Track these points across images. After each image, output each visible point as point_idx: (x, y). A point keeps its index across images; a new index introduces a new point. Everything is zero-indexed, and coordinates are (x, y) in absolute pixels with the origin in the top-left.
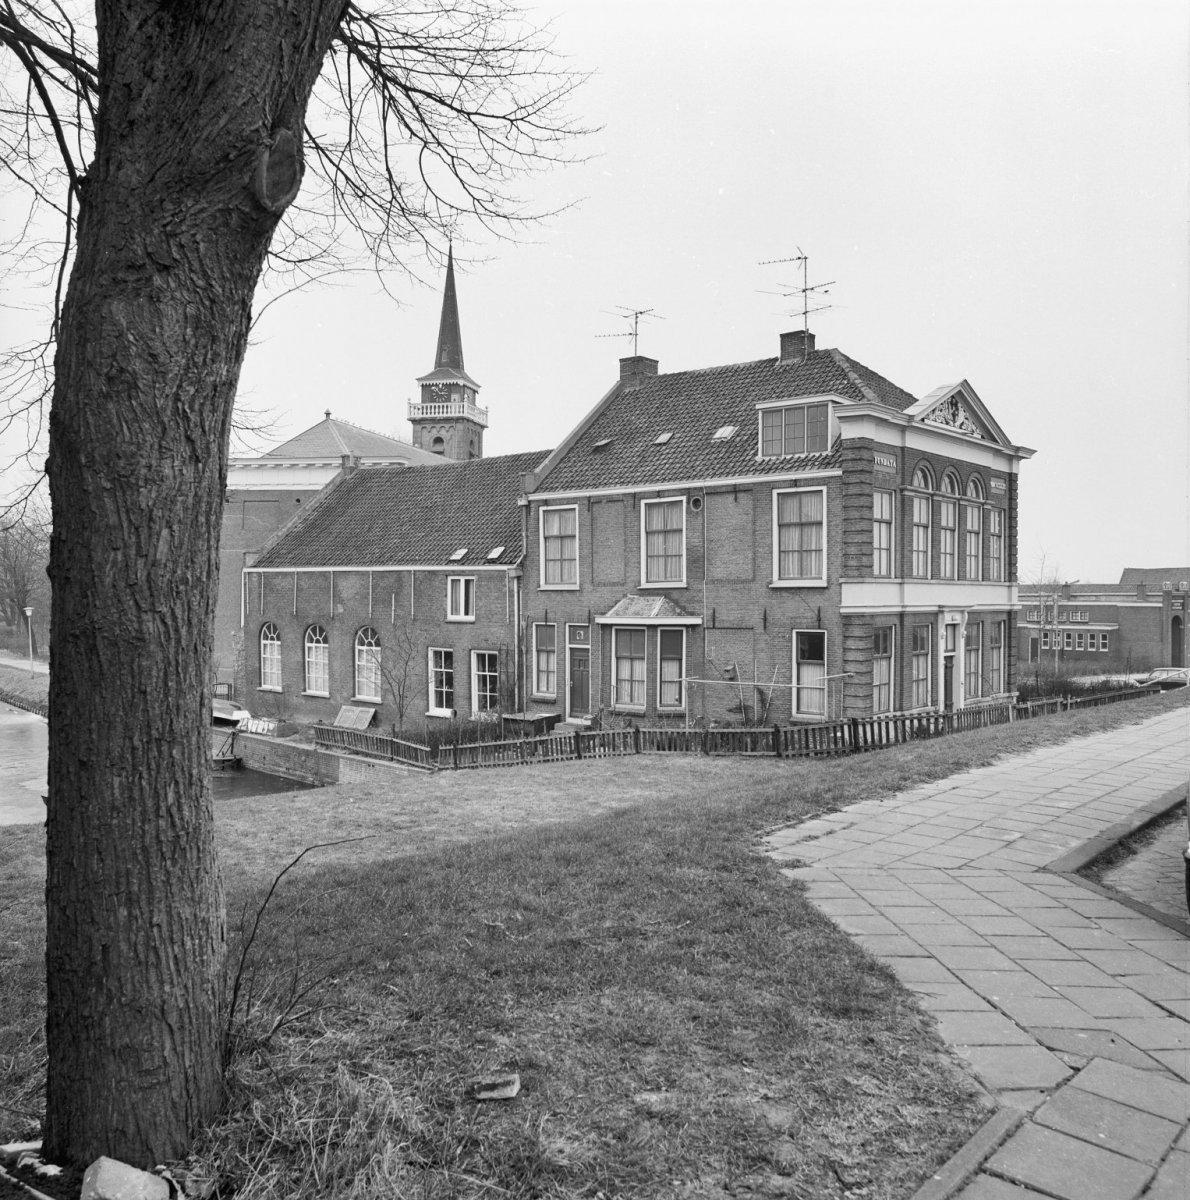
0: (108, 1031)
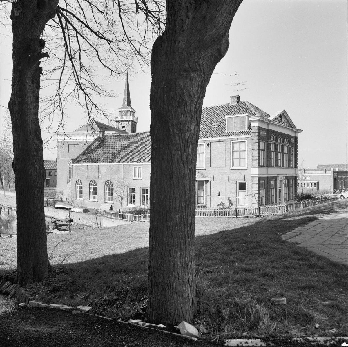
0: (175, 287)
